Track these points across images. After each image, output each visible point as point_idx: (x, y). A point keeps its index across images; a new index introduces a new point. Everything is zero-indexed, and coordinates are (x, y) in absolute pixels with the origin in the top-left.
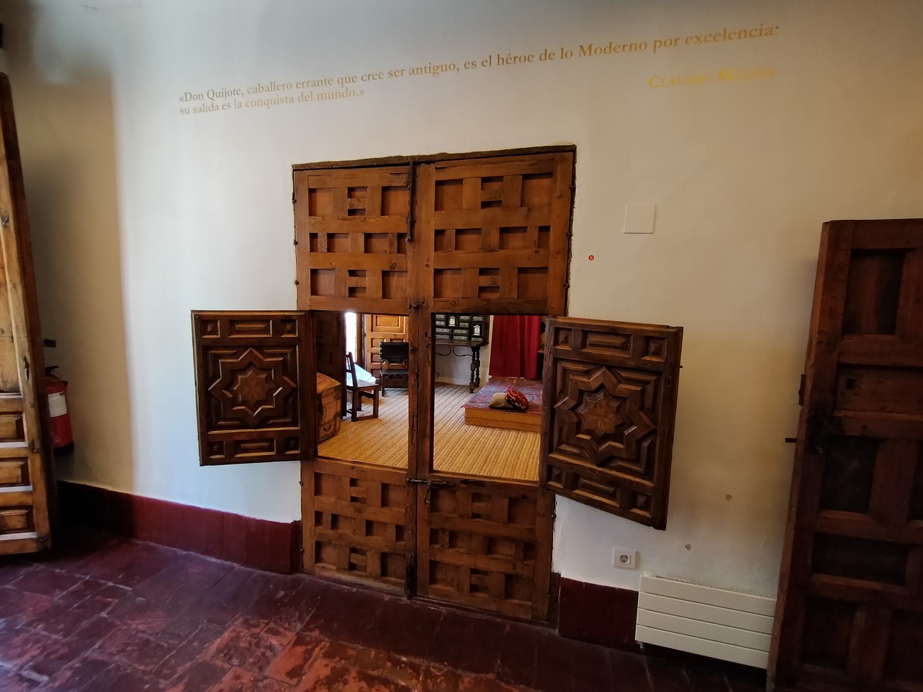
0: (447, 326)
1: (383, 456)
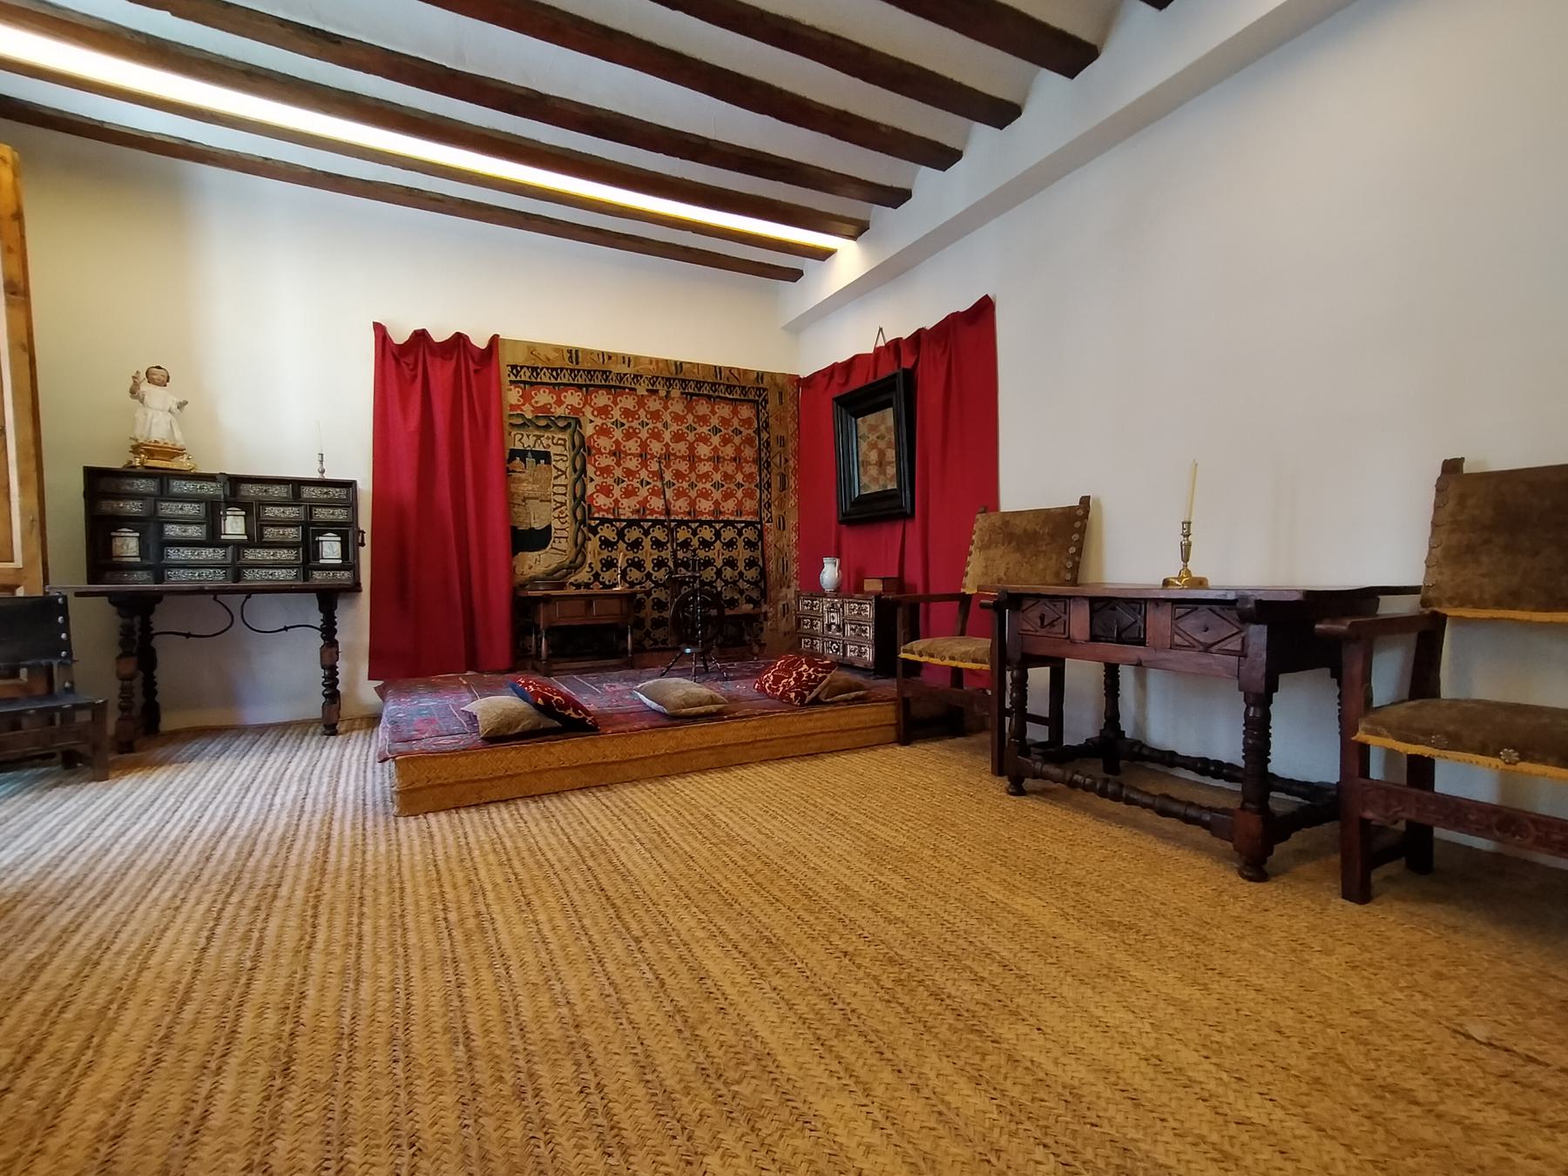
0: (214, 538)
1: (88, 1083)
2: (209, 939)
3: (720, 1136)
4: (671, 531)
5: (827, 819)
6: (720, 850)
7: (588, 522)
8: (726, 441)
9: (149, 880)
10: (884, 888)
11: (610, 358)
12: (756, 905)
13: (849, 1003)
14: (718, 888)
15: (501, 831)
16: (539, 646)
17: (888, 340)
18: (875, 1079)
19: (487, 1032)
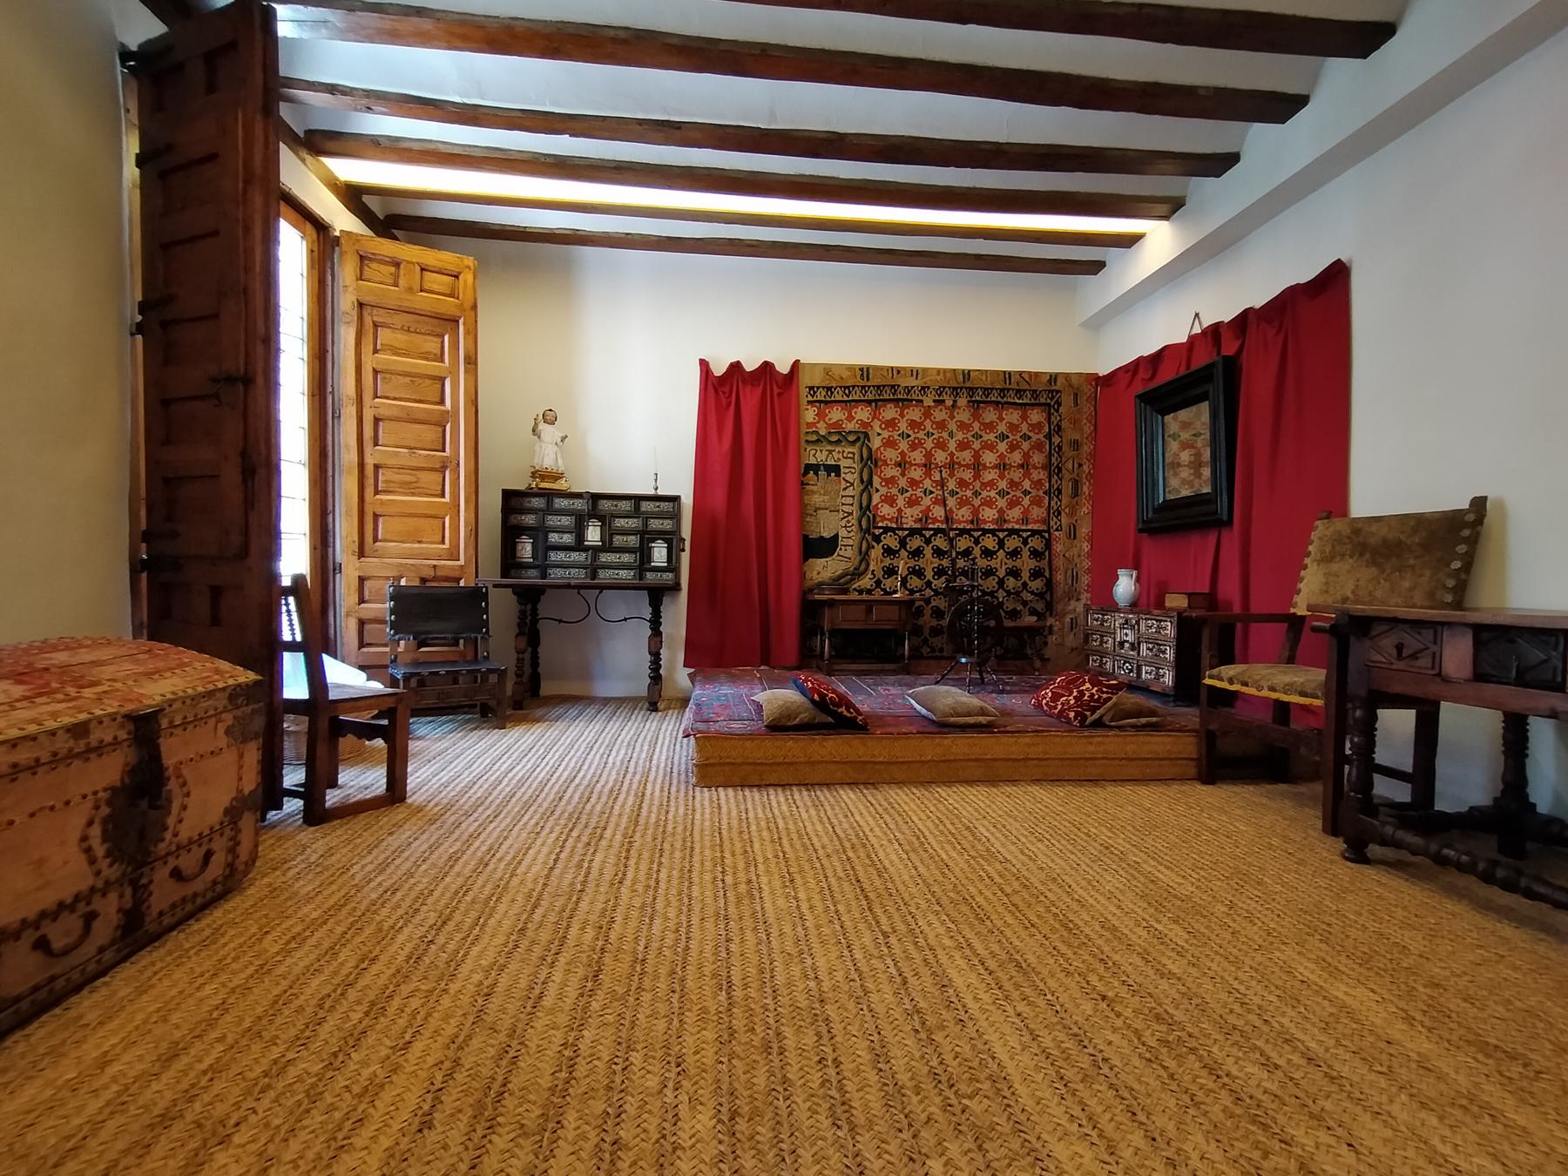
0: (579, 545)
1: (475, 950)
2: (556, 861)
3: (945, 1144)
4: (951, 540)
5: (1101, 852)
6: (978, 863)
7: (872, 530)
8: (1013, 447)
9: (522, 808)
10: (1160, 937)
11: (899, 372)
12: (1009, 925)
13: (1101, 1051)
14: (971, 900)
15: (776, 812)
16: (823, 647)
17: (1205, 325)
18: (1123, 1139)
19: (746, 986)
